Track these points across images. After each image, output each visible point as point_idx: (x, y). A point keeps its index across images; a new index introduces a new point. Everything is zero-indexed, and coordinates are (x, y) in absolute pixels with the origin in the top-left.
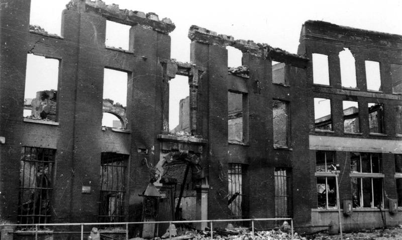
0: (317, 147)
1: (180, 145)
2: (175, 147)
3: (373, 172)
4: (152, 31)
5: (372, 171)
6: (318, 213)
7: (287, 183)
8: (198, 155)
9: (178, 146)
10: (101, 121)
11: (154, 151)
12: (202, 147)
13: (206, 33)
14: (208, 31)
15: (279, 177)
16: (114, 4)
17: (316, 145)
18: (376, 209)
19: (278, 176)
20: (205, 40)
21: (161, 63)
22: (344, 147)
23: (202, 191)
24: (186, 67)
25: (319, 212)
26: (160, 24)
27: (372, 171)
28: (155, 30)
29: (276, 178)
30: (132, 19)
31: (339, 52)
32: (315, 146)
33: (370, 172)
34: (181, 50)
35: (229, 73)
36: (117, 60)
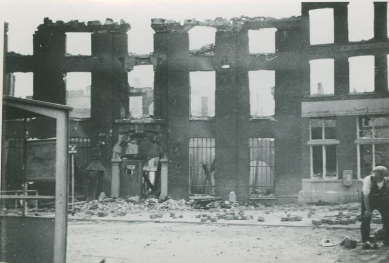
0: (312, 114)
1: (136, 127)
2: (131, 129)
3: (326, 138)
4: (109, 37)
5: (53, 138)
6: (310, 183)
7: (249, 155)
8: (156, 133)
9: (134, 127)
10: (276, 104)
11: (112, 134)
12: (159, 126)
13: (161, 23)
14: (163, 21)
15: (205, 149)
16: (108, 19)
17: (311, 112)
18: (317, 179)
19: (211, 147)
20: (163, 29)
21: (118, 59)
22: (347, 111)
23: (162, 164)
24: (146, 57)
25: (312, 182)
26: (115, 26)
27: (53, 138)
28: (111, 33)
29: (251, 149)
30: (91, 27)
31: (102, 26)
32: (309, 113)
33: (321, 138)
34: (140, 42)
35: (191, 55)
36: (79, 64)
